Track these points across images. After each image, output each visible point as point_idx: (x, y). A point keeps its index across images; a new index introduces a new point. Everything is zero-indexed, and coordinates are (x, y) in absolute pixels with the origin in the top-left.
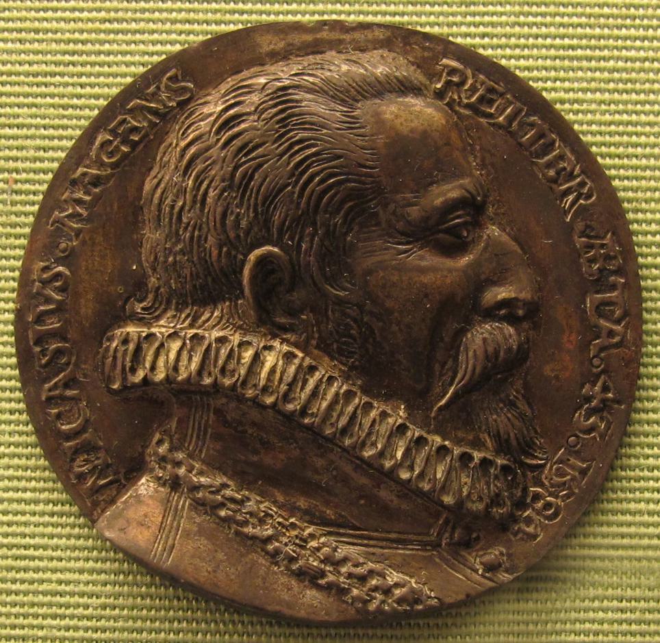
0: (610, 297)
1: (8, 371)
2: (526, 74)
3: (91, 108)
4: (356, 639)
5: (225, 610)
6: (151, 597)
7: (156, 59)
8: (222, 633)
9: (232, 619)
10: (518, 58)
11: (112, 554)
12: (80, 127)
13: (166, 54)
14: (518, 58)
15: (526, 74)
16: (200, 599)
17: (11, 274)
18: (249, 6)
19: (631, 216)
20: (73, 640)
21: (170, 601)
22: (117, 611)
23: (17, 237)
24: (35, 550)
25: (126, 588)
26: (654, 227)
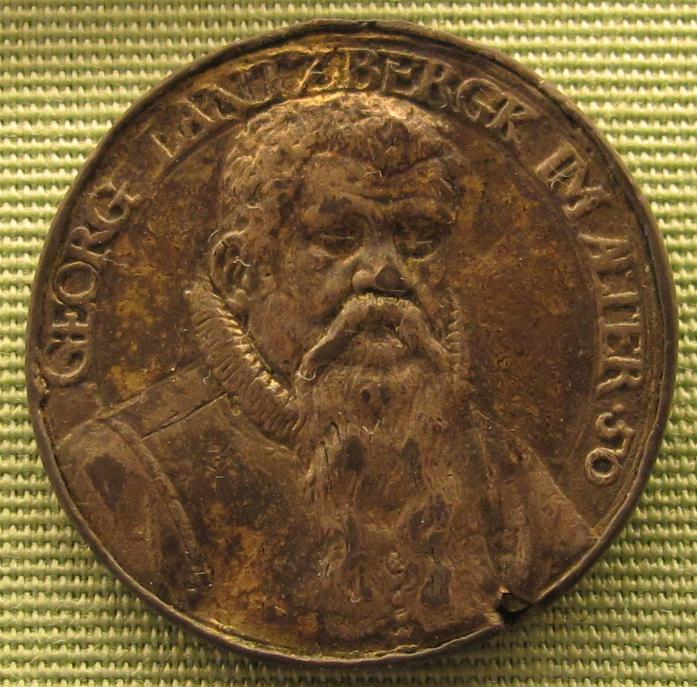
0: (604, 386)
1: (14, 359)
2: (573, 91)
3: (100, 120)
4: (488, 681)
5: (200, 645)
6: (73, 560)
7: (158, 76)
8: (126, 611)
9: (211, 657)
10: (491, 35)
11: (125, 600)
12: (84, 153)
13: (172, 69)
14: (601, 101)
15: (573, 91)
16: (174, 628)
17: (13, 377)
18: (632, 9)
19: (676, 257)
20: (59, 680)
21: (158, 631)
22: (27, 531)
23: (27, 236)
24: (87, 666)
25: (139, 633)
26: (689, 43)
